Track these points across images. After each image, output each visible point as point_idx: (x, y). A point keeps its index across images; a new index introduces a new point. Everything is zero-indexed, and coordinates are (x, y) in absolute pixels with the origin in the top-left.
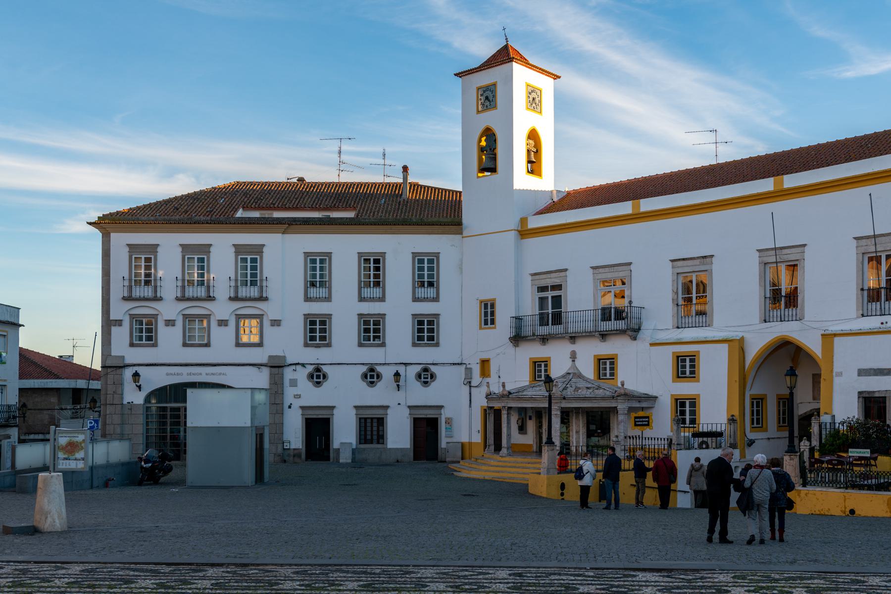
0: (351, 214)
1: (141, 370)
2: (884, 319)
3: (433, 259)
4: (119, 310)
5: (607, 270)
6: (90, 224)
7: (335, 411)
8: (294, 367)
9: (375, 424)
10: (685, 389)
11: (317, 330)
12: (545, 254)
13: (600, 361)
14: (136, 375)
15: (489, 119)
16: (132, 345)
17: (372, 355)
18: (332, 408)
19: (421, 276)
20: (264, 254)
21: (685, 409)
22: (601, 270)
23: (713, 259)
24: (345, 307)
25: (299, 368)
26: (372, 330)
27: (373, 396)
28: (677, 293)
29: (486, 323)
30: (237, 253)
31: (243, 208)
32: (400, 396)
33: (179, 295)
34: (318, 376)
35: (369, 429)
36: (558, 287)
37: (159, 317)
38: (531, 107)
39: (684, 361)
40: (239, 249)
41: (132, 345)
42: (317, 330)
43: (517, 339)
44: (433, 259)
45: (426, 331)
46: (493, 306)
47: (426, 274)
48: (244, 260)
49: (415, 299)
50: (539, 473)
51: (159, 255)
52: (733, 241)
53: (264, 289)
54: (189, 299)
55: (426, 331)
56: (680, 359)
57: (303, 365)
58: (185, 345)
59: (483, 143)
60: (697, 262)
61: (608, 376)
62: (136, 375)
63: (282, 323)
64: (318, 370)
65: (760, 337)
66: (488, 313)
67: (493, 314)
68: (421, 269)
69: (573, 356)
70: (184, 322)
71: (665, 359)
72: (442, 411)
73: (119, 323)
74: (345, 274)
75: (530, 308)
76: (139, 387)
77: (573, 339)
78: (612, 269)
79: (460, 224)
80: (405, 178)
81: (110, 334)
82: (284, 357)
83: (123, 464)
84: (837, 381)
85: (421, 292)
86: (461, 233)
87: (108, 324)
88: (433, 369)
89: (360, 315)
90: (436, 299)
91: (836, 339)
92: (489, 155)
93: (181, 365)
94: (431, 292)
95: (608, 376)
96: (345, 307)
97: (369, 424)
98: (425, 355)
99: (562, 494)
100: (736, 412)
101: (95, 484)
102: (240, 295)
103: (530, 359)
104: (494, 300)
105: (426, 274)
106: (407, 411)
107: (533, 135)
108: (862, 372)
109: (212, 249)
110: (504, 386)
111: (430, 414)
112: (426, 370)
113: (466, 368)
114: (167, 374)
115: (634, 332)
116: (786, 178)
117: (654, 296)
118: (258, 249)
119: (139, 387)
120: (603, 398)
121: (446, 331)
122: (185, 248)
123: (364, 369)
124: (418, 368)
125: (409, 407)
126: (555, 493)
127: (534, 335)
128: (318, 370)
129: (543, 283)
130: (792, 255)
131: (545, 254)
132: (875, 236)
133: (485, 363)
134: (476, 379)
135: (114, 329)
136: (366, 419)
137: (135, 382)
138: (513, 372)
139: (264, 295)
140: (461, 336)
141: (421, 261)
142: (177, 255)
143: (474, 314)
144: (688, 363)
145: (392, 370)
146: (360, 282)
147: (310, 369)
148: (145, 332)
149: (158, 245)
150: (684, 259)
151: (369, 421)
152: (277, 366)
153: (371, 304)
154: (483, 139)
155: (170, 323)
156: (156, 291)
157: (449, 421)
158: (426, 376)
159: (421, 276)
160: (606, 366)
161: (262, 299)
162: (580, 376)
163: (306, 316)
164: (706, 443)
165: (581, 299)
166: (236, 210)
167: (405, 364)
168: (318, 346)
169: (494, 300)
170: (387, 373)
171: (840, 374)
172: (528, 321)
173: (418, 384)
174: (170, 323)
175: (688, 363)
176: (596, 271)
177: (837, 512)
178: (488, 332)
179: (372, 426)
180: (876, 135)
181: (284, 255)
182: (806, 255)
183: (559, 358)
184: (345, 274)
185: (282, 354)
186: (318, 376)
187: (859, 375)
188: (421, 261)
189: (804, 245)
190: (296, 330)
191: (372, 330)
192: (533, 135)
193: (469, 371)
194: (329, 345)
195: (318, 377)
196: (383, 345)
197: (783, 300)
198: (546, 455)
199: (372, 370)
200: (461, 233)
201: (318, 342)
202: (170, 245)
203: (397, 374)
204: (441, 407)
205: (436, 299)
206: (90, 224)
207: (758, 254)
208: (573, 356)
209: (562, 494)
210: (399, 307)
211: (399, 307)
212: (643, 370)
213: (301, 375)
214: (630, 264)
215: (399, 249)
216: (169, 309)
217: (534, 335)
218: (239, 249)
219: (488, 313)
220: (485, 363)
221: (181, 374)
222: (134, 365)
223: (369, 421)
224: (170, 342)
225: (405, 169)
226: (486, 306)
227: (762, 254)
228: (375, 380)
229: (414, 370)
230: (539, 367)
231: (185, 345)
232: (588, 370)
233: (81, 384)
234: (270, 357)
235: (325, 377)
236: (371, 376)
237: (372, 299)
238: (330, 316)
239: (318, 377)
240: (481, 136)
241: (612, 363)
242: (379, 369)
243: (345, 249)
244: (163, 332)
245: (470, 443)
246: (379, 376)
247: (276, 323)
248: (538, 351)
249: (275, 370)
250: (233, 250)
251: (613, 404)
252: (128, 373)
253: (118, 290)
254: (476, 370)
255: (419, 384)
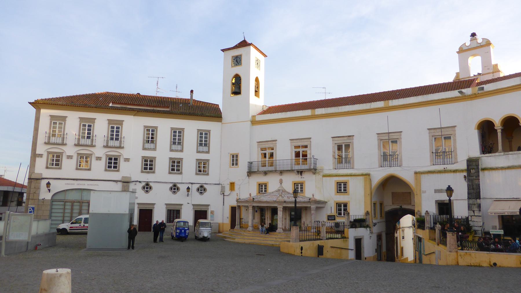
0: (168, 110)
1: (51, 181)
2: (445, 166)
3: (207, 133)
4: (41, 149)
5: (298, 141)
6: (30, 103)
7: (155, 206)
8: (135, 183)
9: (175, 213)
10: (342, 198)
11: (148, 165)
12: (266, 133)
13: (260, 185)
14: (48, 184)
15: (237, 70)
16: (47, 168)
17: (175, 178)
18: (154, 204)
19: (201, 141)
20: (123, 125)
21: (342, 208)
22: (295, 141)
23: (456, 128)
24: (162, 154)
25: (138, 183)
26: (176, 166)
27: (175, 199)
28: (335, 153)
29: (233, 165)
30: (109, 124)
31: (113, 103)
32: (188, 199)
33: (76, 143)
34: (147, 187)
35: (172, 215)
36: (306, 147)
37: (64, 154)
38: (255, 68)
39: (262, 186)
40: (110, 121)
41: (47, 168)
42: (148, 165)
43: (250, 173)
44: (207, 133)
45: (202, 167)
46: (237, 156)
47: (204, 140)
48: (113, 128)
49: (198, 152)
50: (289, 241)
51: (67, 122)
52: (365, 130)
53: (122, 142)
54: (82, 145)
55: (202, 167)
56: (339, 184)
57: (140, 182)
58: (77, 169)
59: (234, 81)
60: (346, 138)
61: (263, 192)
62: (48, 184)
63: (130, 160)
64: (147, 185)
65: (379, 174)
66: (235, 160)
67: (237, 160)
68: (175, 136)
69: (281, 182)
70: (78, 157)
71: (331, 184)
72: (209, 207)
73: (41, 156)
74: (164, 137)
75: (256, 157)
76: (49, 190)
77: (281, 172)
78: (300, 141)
79: (221, 117)
80: (192, 96)
81: (35, 161)
82: (130, 178)
83: (46, 235)
84: (423, 195)
85: (201, 149)
86: (221, 122)
87: (34, 155)
88: (205, 186)
89: (170, 158)
90: (208, 152)
91: (92, 192)
92: (237, 87)
93: (74, 180)
94: (205, 149)
95: (263, 192)
96: (162, 154)
97: (172, 213)
98: (202, 179)
99: (301, 253)
100: (369, 210)
101: (29, 248)
102: (109, 145)
103: (293, 182)
104: (238, 154)
105: (204, 140)
106: (192, 207)
107: (257, 80)
108: (436, 191)
109: (96, 121)
110: (250, 195)
111: (203, 208)
112: (201, 187)
113: (222, 186)
114: (66, 184)
115: (314, 171)
116: (390, 101)
117: (323, 153)
118: (121, 122)
119: (49, 190)
120: (304, 202)
121: (212, 168)
122: (81, 119)
123: (171, 185)
124: (198, 186)
125: (193, 205)
126: (298, 252)
127: (258, 171)
128: (147, 185)
129: (264, 146)
130: (395, 136)
131: (266, 133)
132: (441, 128)
133: (232, 185)
134: (227, 191)
135: (38, 160)
136: (170, 210)
137: (47, 187)
138: (248, 189)
139: (122, 146)
140: (219, 171)
141: (201, 134)
142: (77, 122)
143: (228, 160)
144: (264, 187)
145: (186, 186)
146: (171, 142)
147: (144, 184)
148: (56, 161)
149: (67, 117)
150: (339, 137)
151: (172, 211)
152: (126, 182)
153: (176, 153)
154: (234, 79)
155: (70, 157)
156: (63, 140)
157: (212, 212)
158: (202, 189)
159: (201, 141)
160: (298, 188)
161: (120, 147)
162: (284, 191)
163: (143, 157)
164: (355, 225)
165: (284, 154)
166: (109, 103)
167: (192, 183)
168: (148, 173)
169: (238, 154)
170: (183, 188)
171: (425, 192)
172: (255, 165)
173: (198, 194)
174: (70, 157)
175: (264, 187)
176: (292, 141)
177: (485, 265)
178: (234, 169)
179: (173, 213)
180: (393, 92)
181: (133, 126)
182: (402, 136)
183: (273, 183)
184: (164, 137)
185: (129, 176)
186: (147, 187)
187: (435, 192)
188: (201, 134)
189: (401, 132)
190: (138, 164)
191: (176, 166)
192: (257, 80)
193: (223, 188)
194: (154, 172)
195: (174, 189)
196: (181, 173)
197: (387, 158)
198: (294, 232)
199: (175, 186)
200: (221, 122)
201: (148, 170)
202: (73, 119)
203: (188, 188)
204: (209, 205)
205: (208, 152)
206: (30, 103)
207: (377, 135)
208: (281, 182)
209: (301, 253)
210: (189, 155)
211: (189, 155)
212: (318, 189)
213: (139, 187)
214: (310, 138)
215: (191, 127)
216: (70, 150)
217: (258, 171)
218: (110, 121)
219: (235, 160)
220: (232, 185)
221: (74, 184)
222: (47, 179)
223: (172, 211)
224: (68, 167)
225: (192, 91)
226: (233, 156)
227: (379, 135)
228: (176, 190)
229: (194, 187)
230: (262, 188)
231: (77, 169)
232: (290, 189)
233: (10, 189)
234: (123, 177)
235: (150, 188)
236: (175, 188)
237: (177, 151)
238: (155, 158)
239: (147, 188)
240: (233, 78)
241: (302, 185)
242: (178, 185)
243: (165, 126)
244: (65, 162)
245: (223, 224)
246: (178, 189)
247: (127, 160)
248: (263, 179)
249: (126, 184)
250: (107, 122)
251: (309, 205)
252: (44, 183)
253: (42, 138)
254: (227, 188)
255: (198, 193)
